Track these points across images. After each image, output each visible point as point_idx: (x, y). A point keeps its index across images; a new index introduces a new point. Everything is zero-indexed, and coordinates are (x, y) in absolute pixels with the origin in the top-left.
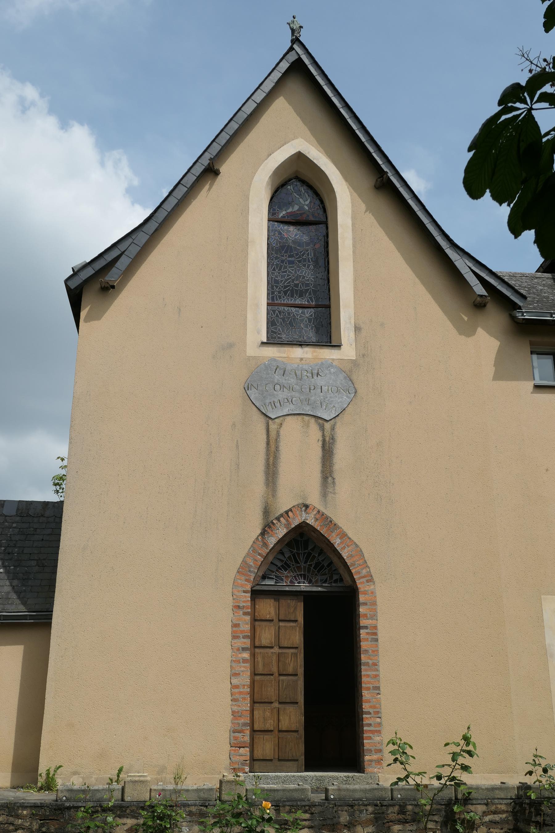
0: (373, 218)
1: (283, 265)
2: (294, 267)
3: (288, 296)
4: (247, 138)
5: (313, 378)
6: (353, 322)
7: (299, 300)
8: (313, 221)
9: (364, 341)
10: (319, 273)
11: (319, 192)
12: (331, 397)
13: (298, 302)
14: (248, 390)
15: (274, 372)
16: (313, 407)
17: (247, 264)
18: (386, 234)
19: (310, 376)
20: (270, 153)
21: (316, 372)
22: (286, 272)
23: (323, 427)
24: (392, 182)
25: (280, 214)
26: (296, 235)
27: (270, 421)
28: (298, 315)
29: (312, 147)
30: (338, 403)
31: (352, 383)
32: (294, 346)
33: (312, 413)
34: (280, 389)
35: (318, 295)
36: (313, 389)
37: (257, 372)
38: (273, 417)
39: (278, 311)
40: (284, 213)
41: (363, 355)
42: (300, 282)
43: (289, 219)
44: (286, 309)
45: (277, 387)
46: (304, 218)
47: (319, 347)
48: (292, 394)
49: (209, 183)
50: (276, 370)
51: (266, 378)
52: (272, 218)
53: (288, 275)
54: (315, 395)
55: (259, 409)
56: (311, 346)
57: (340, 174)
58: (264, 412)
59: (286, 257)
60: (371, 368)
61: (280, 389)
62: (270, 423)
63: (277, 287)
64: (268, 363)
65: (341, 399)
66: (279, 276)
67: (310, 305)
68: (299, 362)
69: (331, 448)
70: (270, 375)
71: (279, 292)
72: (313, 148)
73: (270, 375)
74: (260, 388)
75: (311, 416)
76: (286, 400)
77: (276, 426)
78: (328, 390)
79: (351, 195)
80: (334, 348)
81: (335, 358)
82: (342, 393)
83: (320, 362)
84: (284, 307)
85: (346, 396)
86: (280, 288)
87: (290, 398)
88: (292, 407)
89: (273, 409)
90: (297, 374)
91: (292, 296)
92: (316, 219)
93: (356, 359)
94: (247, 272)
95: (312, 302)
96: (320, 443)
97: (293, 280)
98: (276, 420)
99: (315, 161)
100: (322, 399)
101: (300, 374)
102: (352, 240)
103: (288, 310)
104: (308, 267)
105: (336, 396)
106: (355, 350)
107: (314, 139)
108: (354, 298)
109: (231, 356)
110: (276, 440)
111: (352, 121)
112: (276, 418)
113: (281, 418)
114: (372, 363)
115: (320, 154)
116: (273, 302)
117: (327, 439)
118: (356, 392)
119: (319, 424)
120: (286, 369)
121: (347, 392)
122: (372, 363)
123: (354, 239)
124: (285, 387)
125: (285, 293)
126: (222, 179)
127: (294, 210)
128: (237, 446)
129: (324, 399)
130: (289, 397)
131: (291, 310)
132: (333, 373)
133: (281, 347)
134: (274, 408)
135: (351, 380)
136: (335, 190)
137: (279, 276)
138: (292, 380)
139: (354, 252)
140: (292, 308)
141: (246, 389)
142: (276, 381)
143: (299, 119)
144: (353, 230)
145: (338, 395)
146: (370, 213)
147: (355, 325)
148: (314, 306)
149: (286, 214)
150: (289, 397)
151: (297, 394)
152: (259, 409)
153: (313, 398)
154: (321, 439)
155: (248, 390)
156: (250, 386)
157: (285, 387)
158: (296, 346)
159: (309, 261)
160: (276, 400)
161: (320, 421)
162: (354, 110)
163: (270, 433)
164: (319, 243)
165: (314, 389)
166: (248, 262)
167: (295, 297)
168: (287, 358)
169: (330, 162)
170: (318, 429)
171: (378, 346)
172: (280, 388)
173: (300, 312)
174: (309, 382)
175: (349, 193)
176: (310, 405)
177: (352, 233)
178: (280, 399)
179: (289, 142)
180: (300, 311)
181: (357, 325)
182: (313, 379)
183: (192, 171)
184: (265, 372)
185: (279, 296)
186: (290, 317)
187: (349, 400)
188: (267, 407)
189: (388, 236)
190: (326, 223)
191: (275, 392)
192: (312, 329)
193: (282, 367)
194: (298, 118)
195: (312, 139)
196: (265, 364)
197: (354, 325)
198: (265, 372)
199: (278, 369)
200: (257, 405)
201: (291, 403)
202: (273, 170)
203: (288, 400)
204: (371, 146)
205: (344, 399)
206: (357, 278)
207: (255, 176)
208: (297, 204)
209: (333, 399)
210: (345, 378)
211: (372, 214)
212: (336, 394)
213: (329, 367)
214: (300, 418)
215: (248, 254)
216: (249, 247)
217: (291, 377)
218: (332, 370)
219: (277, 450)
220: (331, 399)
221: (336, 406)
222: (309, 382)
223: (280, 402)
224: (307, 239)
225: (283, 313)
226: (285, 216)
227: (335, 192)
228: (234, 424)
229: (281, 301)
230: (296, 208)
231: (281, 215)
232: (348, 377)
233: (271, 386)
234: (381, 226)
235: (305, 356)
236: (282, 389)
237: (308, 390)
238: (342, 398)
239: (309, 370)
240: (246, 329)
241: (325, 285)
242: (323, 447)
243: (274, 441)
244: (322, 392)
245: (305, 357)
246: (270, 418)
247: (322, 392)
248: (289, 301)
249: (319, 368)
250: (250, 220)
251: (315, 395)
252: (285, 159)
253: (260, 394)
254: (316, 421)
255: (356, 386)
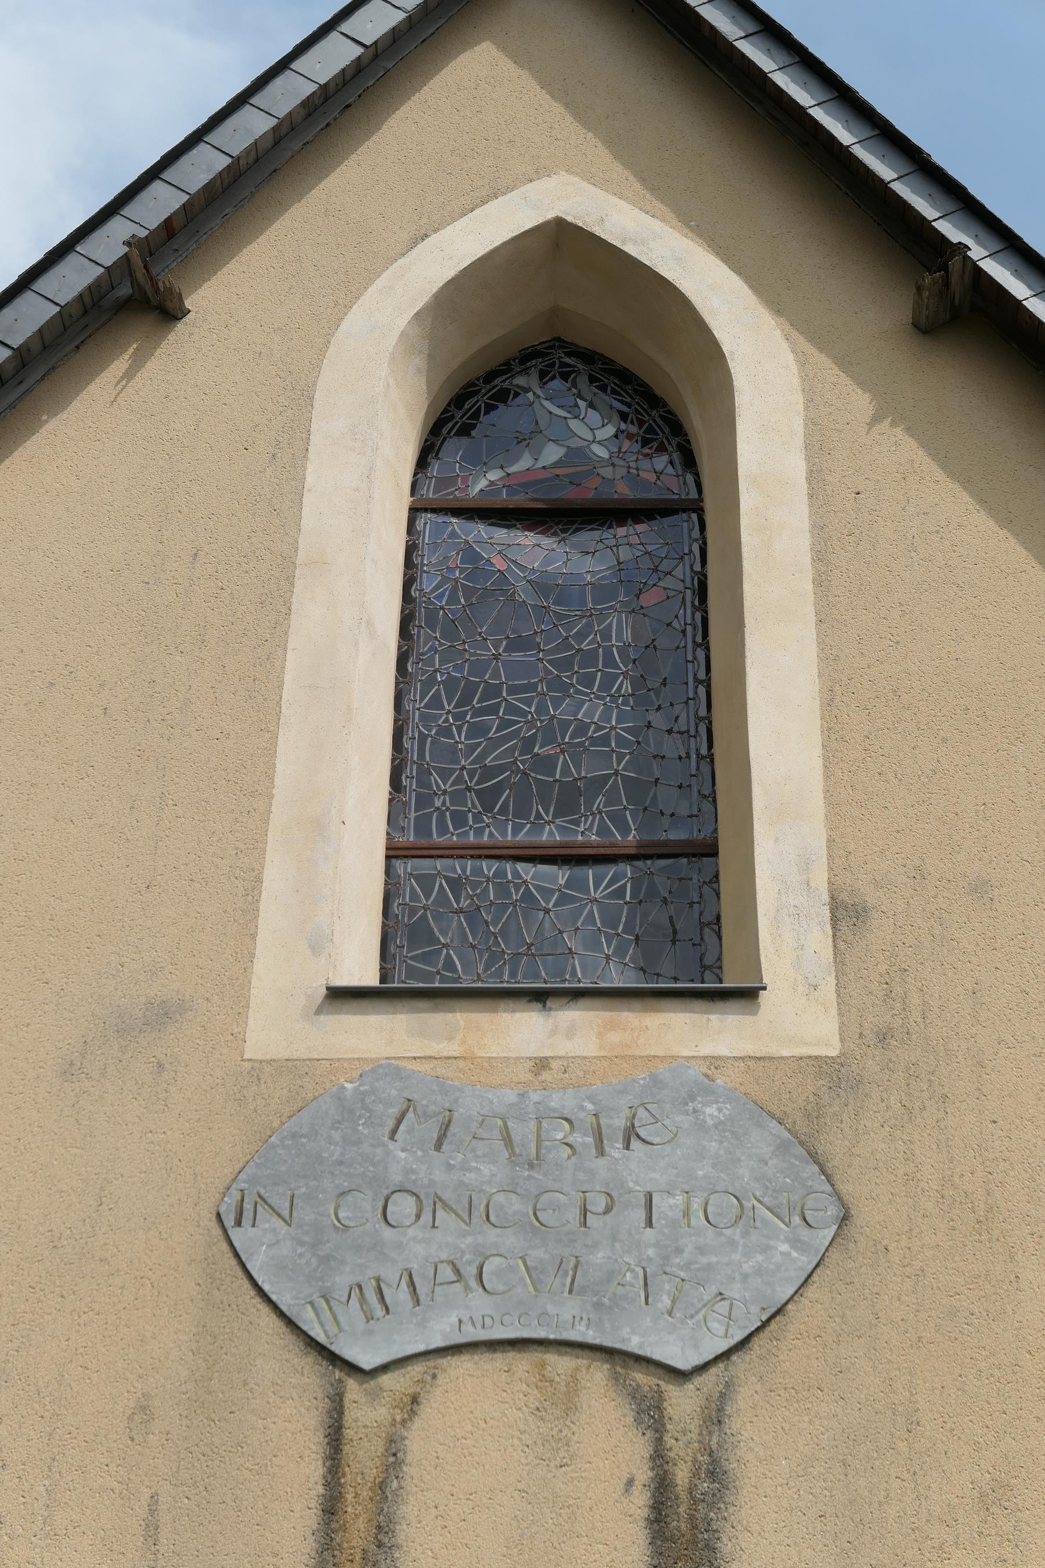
0: (909, 444)
1: (478, 684)
2: (532, 687)
3: (499, 813)
4: (321, 185)
5: (601, 1152)
6: (820, 879)
7: (558, 827)
8: (632, 500)
9: (883, 968)
10: (659, 708)
11: (659, 392)
12: (701, 1250)
13: (550, 835)
14: (239, 1223)
15: (387, 1131)
16: (598, 1306)
17: (280, 652)
18: (982, 501)
19: (585, 1145)
20: (423, 232)
21: (620, 1122)
22: (493, 710)
23: (659, 1408)
24: (1000, 288)
25: (474, 482)
26: (547, 561)
27: (353, 1387)
28: (552, 892)
29: (615, 200)
30: (745, 1277)
31: (823, 1172)
32: (503, 1004)
33: (591, 1336)
34: (418, 1217)
35: (655, 798)
36: (601, 1207)
37: (294, 1136)
38: (367, 1361)
39: (446, 878)
40: (494, 475)
41: (883, 1037)
42: (562, 751)
43: (521, 500)
44: (491, 868)
45: (403, 1207)
46: (588, 493)
47: (637, 1004)
48: (480, 1239)
49: (135, 346)
50: (399, 1122)
51: (340, 1163)
52: (434, 500)
53: (505, 724)
54: (614, 1238)
55: (290, 1323)
56: (597, 1002)
57: (746, 288)
58: (321, 1338)
59: (496, 648)
60: (926, 1094)
61: (418, 1217)
62: (348, 1397)
63: (444, 774)
64: (356, 1089)
65: (760, 1258)
66: (459, 729)
67: (613, 846)
68: (530, 1076)
69: (702, 1527)
70: (366, 1148)
71: (458, 797)
72: (622, 204)
73: (366, 1148)
74: (305, 1214)
75: (586, 1353)
76: (447, 1273)
77: (383, 1410)
78: (687, 1213)
79: (802, 362)
80: (720, 1005)
81: (723, 1051)
82: (766, 1222)
83: (641, 1076)
84: (478, 862)
85: (787, 1240)
86: (459, 780)
87: (469, 1263)
88: (479, 1303)
89: (369, 1318)
90: (516, 1138)
91: (522, 812)
92: (644, 495)
93: (842, 1054)
94: (281, 687)
95: (625, 830)
96: (640, 1501)
97: (528, 745)
98: (386, 1380)
99: (630, 249)
100: (649, 1259)
101: (533, 1138)
102: (808, 535)
103: (500, 873)
104: (606, 686)
105: (732, 1243)
106: (834, 1012)
107: (627, 173)
108: (827, 777)
109: (160, 1065)
110: (382, 1486)
111: (793, 81)
112: (385, 1368)
113: (416, 1369)
114: (933, 1073)
115: (656, 225)
116: (423, 842)
117: (682, 1476)
118: (845, 1219)
119: (635, 1395)
120: (456, 1114)
121: (797, 1220)
122: (933, 1073)
123: (818, 528)
124: (446, 1206)
125: (488, 798)
126: (191, 334)
127: (539, 465)
128: (151, 1530)
129: (666, 1258)
130: (467, 1257)
131: (516, 874)
132: (716, 1126)
133: (435, 1010)
134: (379, 1312)
135: (814, 1157)
136: (726, 349)
137: (459, 729)
138: (486, 1169)
139: (820, 583)
140: (520, 867)
141: (229, 1221)
142: (396, 1177)
143: (563, 110)
144: (811, 496)
145: (745, 1234)
146: (893, 424)
147: (832, 898)
148: (633, 851)
149: (501, 479)
150: (467, 1257)
151: (511, 1240)
152: (290, 1323)
153: (600, 1256)
154: (644, 1474)
155: (239, 1223)
156: (248, 1206)
157: (446, 1206)
158: (511, 1004)
159: (609, 661)
160: (391, 1273)
161: (641, 1378)
162: (800, 35)
163: (346, 1449)
164: (661, 584)
165: (608, 1210)
166: (290, 646)
167: (538, 816)
168: (461, 1064)
169: (700, 249)
170: (630, 1420)
171: (960, 989)
172: (414, 1211)
173: (562, 882)
174: (581, 1176)
175: (791, 357)
176: (583, 1291)
177: (810, 506)
178: (414, 1266)
179: (509, 189)
180: (561, 875)
181: (844, 896)
182: (601, 1162)
183: (44, 284)
184: (337, 1136)
185: (454, 814)
186: (505, 907)
187: (807, 1262)
188: (338, 1309)
189: (992, 511)
190: (697, 508)
191: (388, 1233)
192: (621, 951)
193: (432, 1107)
194: (558, 108)
195: (618, 172)
196: (339, 1096)
197: (826, 897)
198: (337, 1136)
199: (410, 1115)
200: (284, 1301)
201: (473, 1283)
202: (434, 290)
203: (457, 1271)
204: (882, 158)
205: (778, 1258)
206: (837, 688)
207: (350, 315)
208: (553, 441)
209: (714, 1259)
210: (782, 1148)
211: (908, 430)
212: (736, 1233)
213: (692, 1097)
214: (522, 1362)
215: (288, 614)
216: (298, 583)
217: (479, 1153)
218: (711, 1110)
219: (380, 1545)
220: (704, 1260)
221: (734, 1291)
222: (581, 1176)
223: (412, 1284)
224: (601, 571)
225: (475, 885)
226: (500, 490)
227: (722, 356)
228: (144, 1408)
229: (466, 833)
230: (552, 454)
231: (482, 484)
232: (802, 1143)
233: (366, 1203)
234: (952, 474)
235: (565, 1047)
236: (427, 1217)
237: (573, 1215)
238: (766, 1249)
239: (582, 1115)
240: (253, 936)
241: (688, 756)
242: (657, 1521)
243: (365, 1494)
244: (649, 1223)
245: (562, 1053)
246: (352, 1368)
247: (649, 1223)
248: (504, 834)
249: (636, 1103)
250: (310, 479)
251: (614, 1238)
252: (491, 247)
253: (302, 1243)
254: (615, 1377)
255: (844, 1188)
